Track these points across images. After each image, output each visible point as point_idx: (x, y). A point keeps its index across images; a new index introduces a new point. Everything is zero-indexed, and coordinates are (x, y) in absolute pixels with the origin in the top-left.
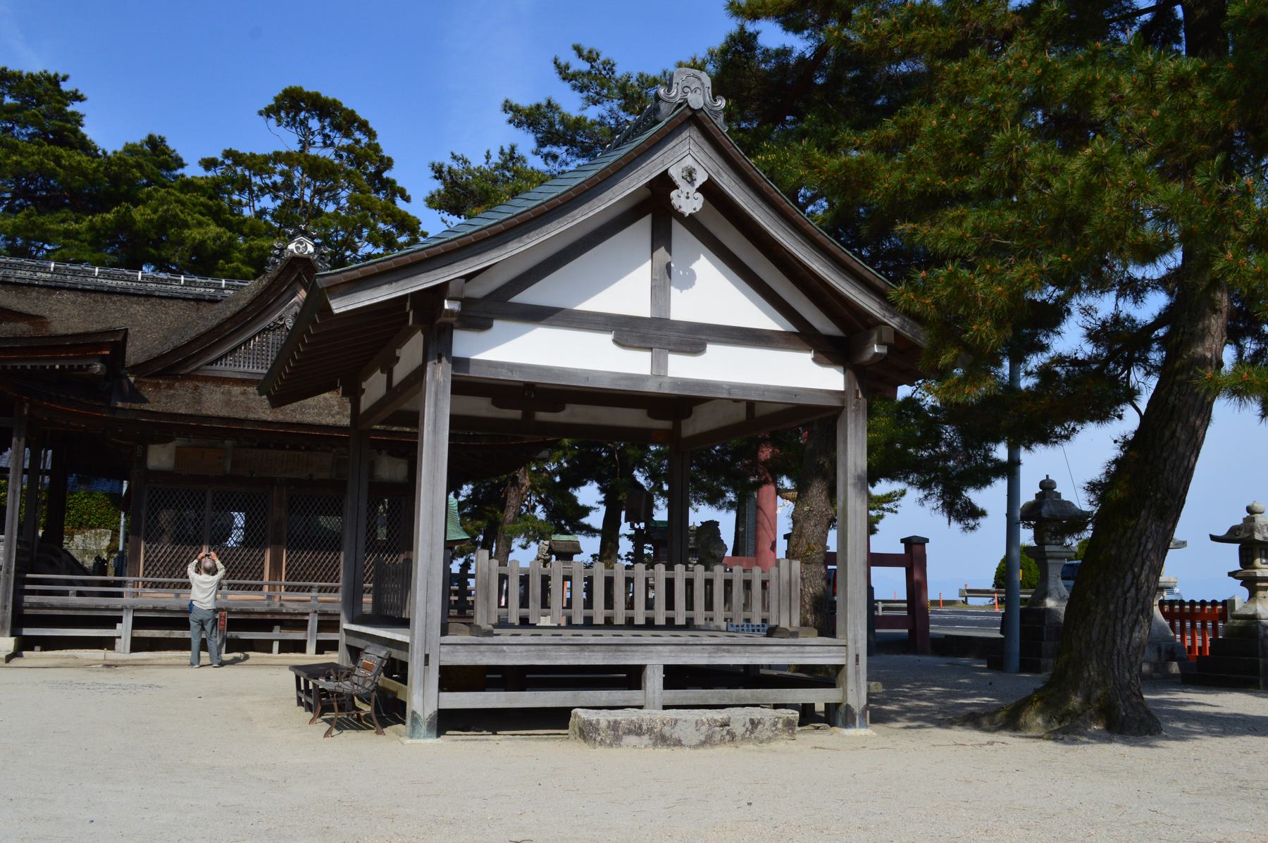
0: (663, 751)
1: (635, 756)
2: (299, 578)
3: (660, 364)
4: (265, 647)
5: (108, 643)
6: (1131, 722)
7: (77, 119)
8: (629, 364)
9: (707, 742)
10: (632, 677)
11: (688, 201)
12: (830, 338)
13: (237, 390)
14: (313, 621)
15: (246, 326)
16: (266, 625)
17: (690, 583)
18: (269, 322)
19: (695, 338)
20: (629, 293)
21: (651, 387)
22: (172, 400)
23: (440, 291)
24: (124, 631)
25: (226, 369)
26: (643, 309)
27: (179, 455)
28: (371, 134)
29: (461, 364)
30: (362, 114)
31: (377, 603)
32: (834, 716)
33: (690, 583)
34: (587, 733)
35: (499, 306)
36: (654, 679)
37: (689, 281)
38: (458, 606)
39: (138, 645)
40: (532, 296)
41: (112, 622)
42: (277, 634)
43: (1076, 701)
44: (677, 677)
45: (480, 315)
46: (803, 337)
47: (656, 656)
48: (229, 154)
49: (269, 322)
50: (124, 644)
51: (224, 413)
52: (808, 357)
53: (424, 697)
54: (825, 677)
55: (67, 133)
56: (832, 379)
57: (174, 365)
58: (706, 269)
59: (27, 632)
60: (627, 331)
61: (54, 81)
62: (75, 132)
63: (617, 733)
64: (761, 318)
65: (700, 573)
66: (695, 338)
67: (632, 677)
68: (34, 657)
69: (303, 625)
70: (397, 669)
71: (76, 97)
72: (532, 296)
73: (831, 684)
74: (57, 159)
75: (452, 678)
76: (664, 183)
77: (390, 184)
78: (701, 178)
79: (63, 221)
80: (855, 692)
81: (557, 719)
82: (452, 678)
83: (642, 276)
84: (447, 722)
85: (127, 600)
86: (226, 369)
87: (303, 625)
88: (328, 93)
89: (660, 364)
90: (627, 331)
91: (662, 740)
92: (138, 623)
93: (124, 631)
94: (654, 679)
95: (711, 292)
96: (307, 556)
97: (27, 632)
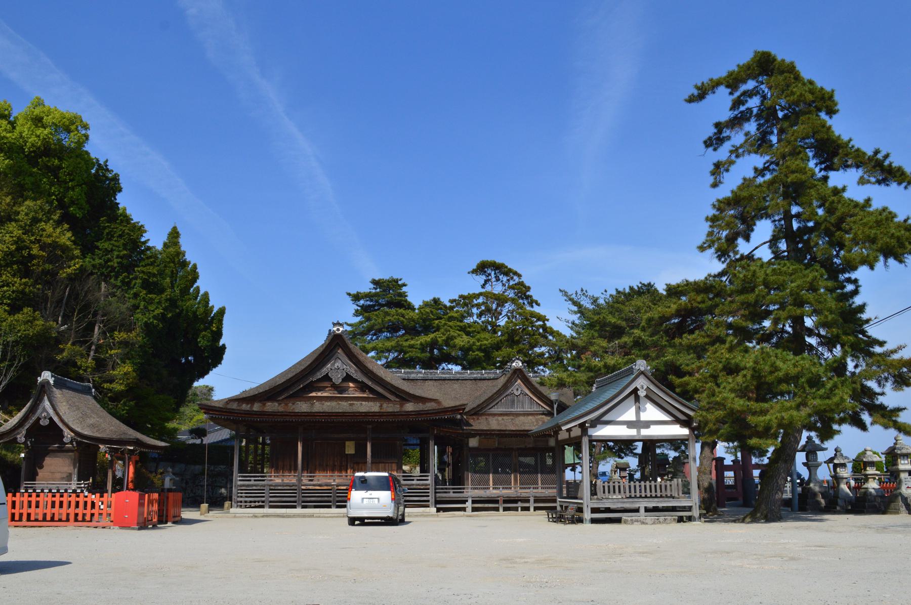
0: (643, 526)
1: (637, 527)
2: (524, 484)
3: (639, 432)
4: (516, 509)
5: (464, 509)
6: (770, 518)
7: (404, 295)
9: (654, 523)
10: (637, 510)
11: (642, 393)
12: (684, 421)
13: (500, 418)
14: (532, 500)
15: (501, 395)
16: (515, 501)
17: (635, 486)
18: (508, 392)
19: (647, 424)
20: (630, 415)
22: (479, 424)
23: (585, 422)
24: (469, 505)
25: (495, 410)
26: (634, 418)
27: (480, 442)
28: (519, 276)
29: (590, 436)
30: (515, 268)
31: (568, 492)
32: (690, 519)
33: (635, 486)
34: (626, 522)
35: (598, 422)
36: (642, 510)
37: (645, 410)
38: (594, 493)
39: (474, 510)
40: (605, 418)
41: (464, 502)
42: (520, 504)
43: (758, 515)
44: (647, 510)
45: (596, 423)
46: (677, 421)
47: (642, 504)
48: (461, 296)
49: (508, 392)
50: (469, 509)
51: (498, 428)
52: (678, 426)
53: (587, 515)
54: (690, 509)
55: (402, 303)
56: (685, 431)
57: (478, 411)
58: (649, 406)
59: (438, 506)
60: (630, 424)
61: (396, 281)
62: (406, 301)
63: (632, 522)
64: (664, 417)
65: (653, 483)
66: (647, 424)
67: (637, 510)
68: (441, 513)
69: (528, 501)
70: (580, 510)
71: (404, 285)
72: (605, 418)
73: (690, 511)
74: (403, 316)
75: (594, 511)
76: (636, 390)
77: (528, 297)
78: (645, 387)
79: (407, 340)
80: (696, 512)
81: (618, 521)
82: (594, 511)
83: (633, 410)
84: (594, 521)
85: (469, 494)
86: (495, 410)
87: (528, 501)
88: (499, 260)
89: (639, 432)
90: (630, 424)
91: (643, 523)
92: (474, 502)
93: (469, 505)
94: (642, 510)
95: (651, 412)
96: (526, 476)
97: (438, 506)
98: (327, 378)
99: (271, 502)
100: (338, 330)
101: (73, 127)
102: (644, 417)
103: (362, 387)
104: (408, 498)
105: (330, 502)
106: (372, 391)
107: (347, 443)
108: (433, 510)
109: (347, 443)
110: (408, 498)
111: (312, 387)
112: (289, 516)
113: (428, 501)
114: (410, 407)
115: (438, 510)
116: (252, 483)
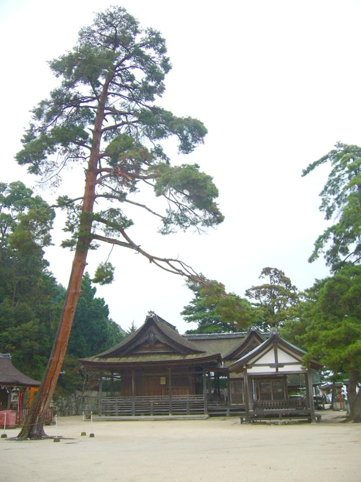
8: (274, 370)
19: (282, 365)
21: (276, 374)
26: (273, 362)
41: (226, 410)
59: (210, 413)
60: (271, 365)
66: (282, 365)
89: (277, 370)
90: (271, 365)
93: (228, 412)
95: (283, 358)
98: (146, 342)
99: (154, 412)
100: (151, 315)
101: (326, 202)
102: (280, 361)
103: (166, 346)
104: (155, 410)
105: (150, 412)
106: (171, 348)
107: (161, 378)
108: (207, 416)
109: (161, 378)
110: (155, 410)
111: (135, 349)
112: (137, 420)
113: (203, 411)
114: (189, 357)
115: (211, 416)
116: (196, 400)
